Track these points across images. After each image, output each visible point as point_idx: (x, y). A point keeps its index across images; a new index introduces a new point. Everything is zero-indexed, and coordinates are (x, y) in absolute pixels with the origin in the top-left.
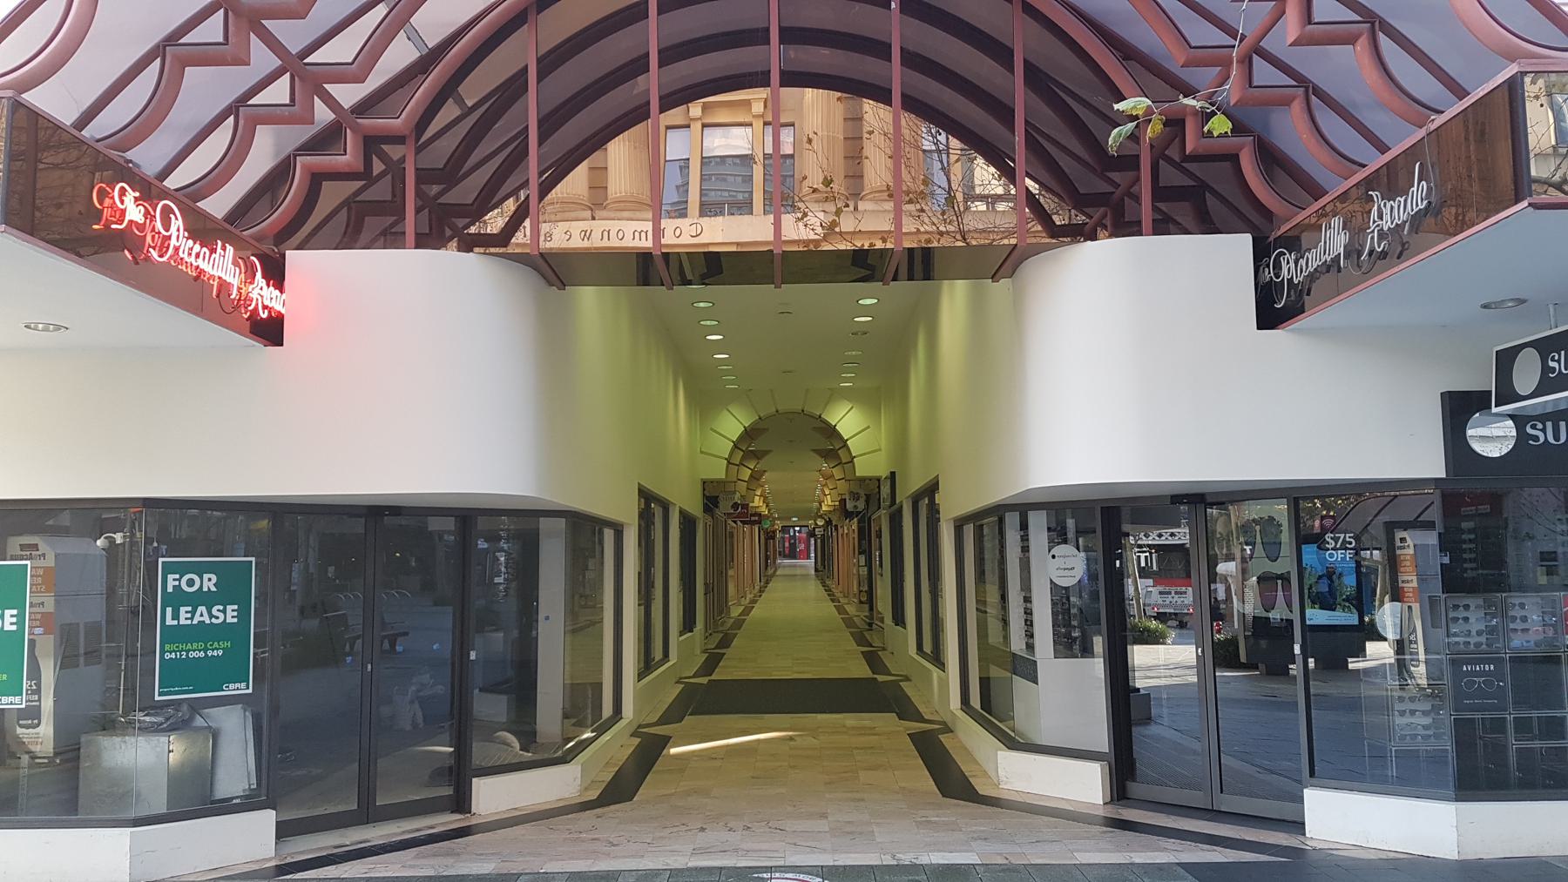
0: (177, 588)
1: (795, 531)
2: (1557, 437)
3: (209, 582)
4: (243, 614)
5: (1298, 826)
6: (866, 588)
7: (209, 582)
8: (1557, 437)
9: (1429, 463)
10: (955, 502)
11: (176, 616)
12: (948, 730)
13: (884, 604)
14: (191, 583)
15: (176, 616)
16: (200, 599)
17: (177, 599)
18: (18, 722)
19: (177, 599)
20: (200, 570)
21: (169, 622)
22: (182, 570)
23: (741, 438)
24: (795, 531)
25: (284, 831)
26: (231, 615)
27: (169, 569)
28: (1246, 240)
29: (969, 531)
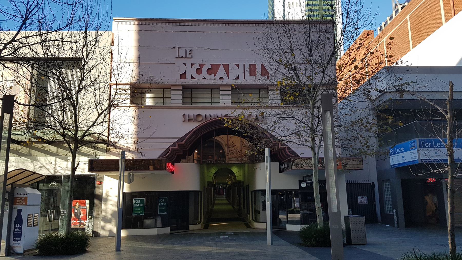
0: (135, 202)
1: (220, 187)
2: (310, 185)
3: (139, 201)
4: (166, 204)
5: (286, 229)
6: (238, 202)
7: (139, 201)
8: (310, 185)
9: (297, 188)
10: (251, 189)
11: (135, 205)
12: (250, 223)
13: (242, 206)
14: (137, 202)
15: (135, 205)
16: (163, 202)
17: (160, 202)
18: (13, 239)
19: (160, 202)
20: (138, 200)
21: (134, 206)
22: (136, 200)
23: (215, 173)
24: (220, 187)
25: (171, 230)
26: (142, 205)
27: (160, 199)
28: (278, 163)
29: (253, 193)
